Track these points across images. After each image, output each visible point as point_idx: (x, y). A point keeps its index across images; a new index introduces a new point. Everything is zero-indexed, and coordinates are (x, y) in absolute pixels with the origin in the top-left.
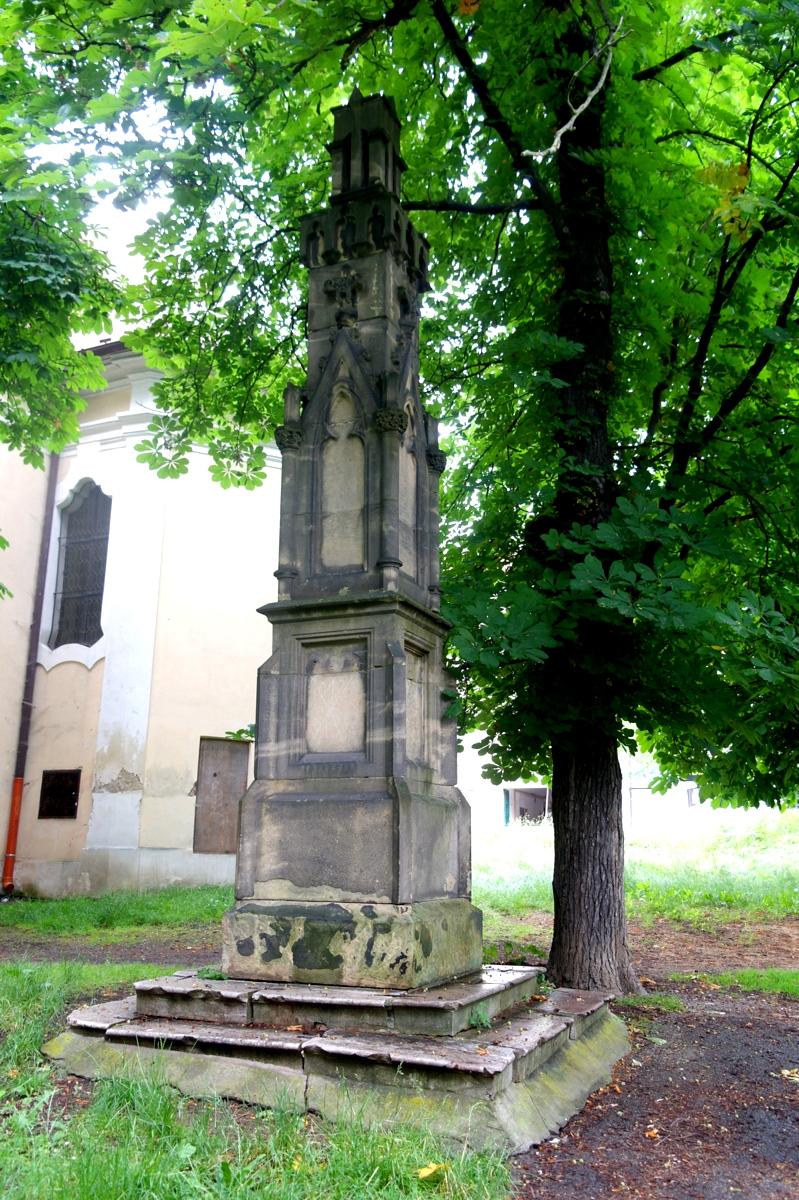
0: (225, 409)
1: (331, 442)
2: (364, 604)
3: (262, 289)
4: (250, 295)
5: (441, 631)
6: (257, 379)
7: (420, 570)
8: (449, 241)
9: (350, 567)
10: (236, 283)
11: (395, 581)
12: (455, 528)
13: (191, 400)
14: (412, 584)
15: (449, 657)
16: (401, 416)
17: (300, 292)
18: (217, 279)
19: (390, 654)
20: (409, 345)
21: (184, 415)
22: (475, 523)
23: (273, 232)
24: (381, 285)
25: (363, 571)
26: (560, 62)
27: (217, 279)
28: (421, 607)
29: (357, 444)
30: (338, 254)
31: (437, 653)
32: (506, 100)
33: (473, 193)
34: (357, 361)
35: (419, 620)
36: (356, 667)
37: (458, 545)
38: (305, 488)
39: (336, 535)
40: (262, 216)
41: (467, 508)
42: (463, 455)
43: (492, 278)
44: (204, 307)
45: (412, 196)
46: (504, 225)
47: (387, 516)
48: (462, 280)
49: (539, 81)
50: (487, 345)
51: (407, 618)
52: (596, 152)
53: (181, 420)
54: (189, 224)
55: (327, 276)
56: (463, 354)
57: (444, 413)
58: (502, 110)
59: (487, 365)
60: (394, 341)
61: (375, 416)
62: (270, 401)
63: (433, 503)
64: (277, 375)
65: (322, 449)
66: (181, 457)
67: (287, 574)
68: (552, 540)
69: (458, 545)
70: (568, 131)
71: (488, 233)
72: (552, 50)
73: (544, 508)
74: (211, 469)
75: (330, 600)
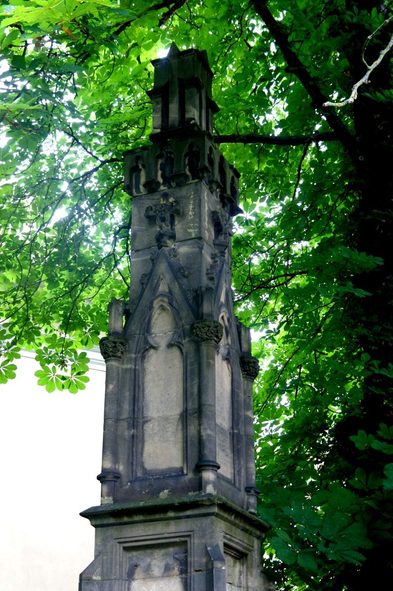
0: (52, 319)
1: (152, 352)
2: (183, 507)
3: (88, 211)
4: (77, 216)
5: (258, 533)
6: (81, 291)
7: (237, 472)
8: (256, 168)
9: (170, 470)
10: (64, 207)
11: (214, 484)
12: (267, 427)
13: (21, 310)
14: (230, 487)
15: (266, 556)
16: (216, 327)
17: (122, 214)
18: (48, 203)
19: (211, 557)
20: (223, 262)
21: (14, 324)
22: (286, 422)
23: (98, 163)
24: (197, 210)
25: (183, 474)
26: (352, 17)
27: (48, 203)
28: (239, 509)
29: (176, 352)
30: (158, 184)
31: (255, 555)
32: (304, 51)
33: (276, 127)
34: (176, 278)
35: (237, 522)
36: (176, 571)
37: (270, 443)
38: (127, 394)
39: (157, 439)
40: (89, 150)
41: (278, 407)
42: (272, 358)
43: (295, 201)
44: (35, 227)
45: (222, 131)
46: (305, 154)
47: (204, 420)
48: (268, 202)
49: (333, 33)
50: (293, 257)
51: (225, 520)
52: (386, 92)
53: (11, 330)
54: (23, 157)
55: (148, 203)
56: (270, 266)
57: (254, 319)
58: (301, 58)
59: (293, 276)
60: (209, 259)
61: (192, 327)
62: (93, 310)
63: (248, 407)
64: (100, 287)
65: (143, 358)
66: (10, 363)
67: (110, 477)
68: (360, 440)
69: (270, 443)
70: (364, 84)
71: (290, 161)
72: (344, 7)
73: (352, 409)
74: (37, 374)
75: (151, 503)
